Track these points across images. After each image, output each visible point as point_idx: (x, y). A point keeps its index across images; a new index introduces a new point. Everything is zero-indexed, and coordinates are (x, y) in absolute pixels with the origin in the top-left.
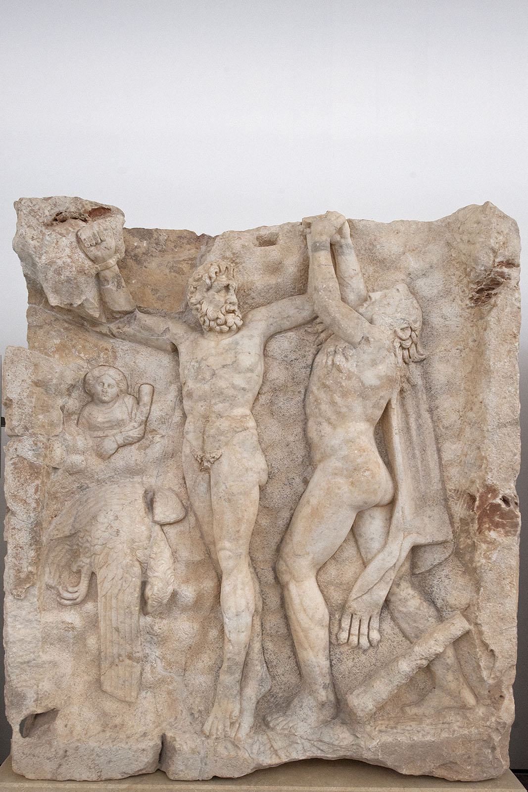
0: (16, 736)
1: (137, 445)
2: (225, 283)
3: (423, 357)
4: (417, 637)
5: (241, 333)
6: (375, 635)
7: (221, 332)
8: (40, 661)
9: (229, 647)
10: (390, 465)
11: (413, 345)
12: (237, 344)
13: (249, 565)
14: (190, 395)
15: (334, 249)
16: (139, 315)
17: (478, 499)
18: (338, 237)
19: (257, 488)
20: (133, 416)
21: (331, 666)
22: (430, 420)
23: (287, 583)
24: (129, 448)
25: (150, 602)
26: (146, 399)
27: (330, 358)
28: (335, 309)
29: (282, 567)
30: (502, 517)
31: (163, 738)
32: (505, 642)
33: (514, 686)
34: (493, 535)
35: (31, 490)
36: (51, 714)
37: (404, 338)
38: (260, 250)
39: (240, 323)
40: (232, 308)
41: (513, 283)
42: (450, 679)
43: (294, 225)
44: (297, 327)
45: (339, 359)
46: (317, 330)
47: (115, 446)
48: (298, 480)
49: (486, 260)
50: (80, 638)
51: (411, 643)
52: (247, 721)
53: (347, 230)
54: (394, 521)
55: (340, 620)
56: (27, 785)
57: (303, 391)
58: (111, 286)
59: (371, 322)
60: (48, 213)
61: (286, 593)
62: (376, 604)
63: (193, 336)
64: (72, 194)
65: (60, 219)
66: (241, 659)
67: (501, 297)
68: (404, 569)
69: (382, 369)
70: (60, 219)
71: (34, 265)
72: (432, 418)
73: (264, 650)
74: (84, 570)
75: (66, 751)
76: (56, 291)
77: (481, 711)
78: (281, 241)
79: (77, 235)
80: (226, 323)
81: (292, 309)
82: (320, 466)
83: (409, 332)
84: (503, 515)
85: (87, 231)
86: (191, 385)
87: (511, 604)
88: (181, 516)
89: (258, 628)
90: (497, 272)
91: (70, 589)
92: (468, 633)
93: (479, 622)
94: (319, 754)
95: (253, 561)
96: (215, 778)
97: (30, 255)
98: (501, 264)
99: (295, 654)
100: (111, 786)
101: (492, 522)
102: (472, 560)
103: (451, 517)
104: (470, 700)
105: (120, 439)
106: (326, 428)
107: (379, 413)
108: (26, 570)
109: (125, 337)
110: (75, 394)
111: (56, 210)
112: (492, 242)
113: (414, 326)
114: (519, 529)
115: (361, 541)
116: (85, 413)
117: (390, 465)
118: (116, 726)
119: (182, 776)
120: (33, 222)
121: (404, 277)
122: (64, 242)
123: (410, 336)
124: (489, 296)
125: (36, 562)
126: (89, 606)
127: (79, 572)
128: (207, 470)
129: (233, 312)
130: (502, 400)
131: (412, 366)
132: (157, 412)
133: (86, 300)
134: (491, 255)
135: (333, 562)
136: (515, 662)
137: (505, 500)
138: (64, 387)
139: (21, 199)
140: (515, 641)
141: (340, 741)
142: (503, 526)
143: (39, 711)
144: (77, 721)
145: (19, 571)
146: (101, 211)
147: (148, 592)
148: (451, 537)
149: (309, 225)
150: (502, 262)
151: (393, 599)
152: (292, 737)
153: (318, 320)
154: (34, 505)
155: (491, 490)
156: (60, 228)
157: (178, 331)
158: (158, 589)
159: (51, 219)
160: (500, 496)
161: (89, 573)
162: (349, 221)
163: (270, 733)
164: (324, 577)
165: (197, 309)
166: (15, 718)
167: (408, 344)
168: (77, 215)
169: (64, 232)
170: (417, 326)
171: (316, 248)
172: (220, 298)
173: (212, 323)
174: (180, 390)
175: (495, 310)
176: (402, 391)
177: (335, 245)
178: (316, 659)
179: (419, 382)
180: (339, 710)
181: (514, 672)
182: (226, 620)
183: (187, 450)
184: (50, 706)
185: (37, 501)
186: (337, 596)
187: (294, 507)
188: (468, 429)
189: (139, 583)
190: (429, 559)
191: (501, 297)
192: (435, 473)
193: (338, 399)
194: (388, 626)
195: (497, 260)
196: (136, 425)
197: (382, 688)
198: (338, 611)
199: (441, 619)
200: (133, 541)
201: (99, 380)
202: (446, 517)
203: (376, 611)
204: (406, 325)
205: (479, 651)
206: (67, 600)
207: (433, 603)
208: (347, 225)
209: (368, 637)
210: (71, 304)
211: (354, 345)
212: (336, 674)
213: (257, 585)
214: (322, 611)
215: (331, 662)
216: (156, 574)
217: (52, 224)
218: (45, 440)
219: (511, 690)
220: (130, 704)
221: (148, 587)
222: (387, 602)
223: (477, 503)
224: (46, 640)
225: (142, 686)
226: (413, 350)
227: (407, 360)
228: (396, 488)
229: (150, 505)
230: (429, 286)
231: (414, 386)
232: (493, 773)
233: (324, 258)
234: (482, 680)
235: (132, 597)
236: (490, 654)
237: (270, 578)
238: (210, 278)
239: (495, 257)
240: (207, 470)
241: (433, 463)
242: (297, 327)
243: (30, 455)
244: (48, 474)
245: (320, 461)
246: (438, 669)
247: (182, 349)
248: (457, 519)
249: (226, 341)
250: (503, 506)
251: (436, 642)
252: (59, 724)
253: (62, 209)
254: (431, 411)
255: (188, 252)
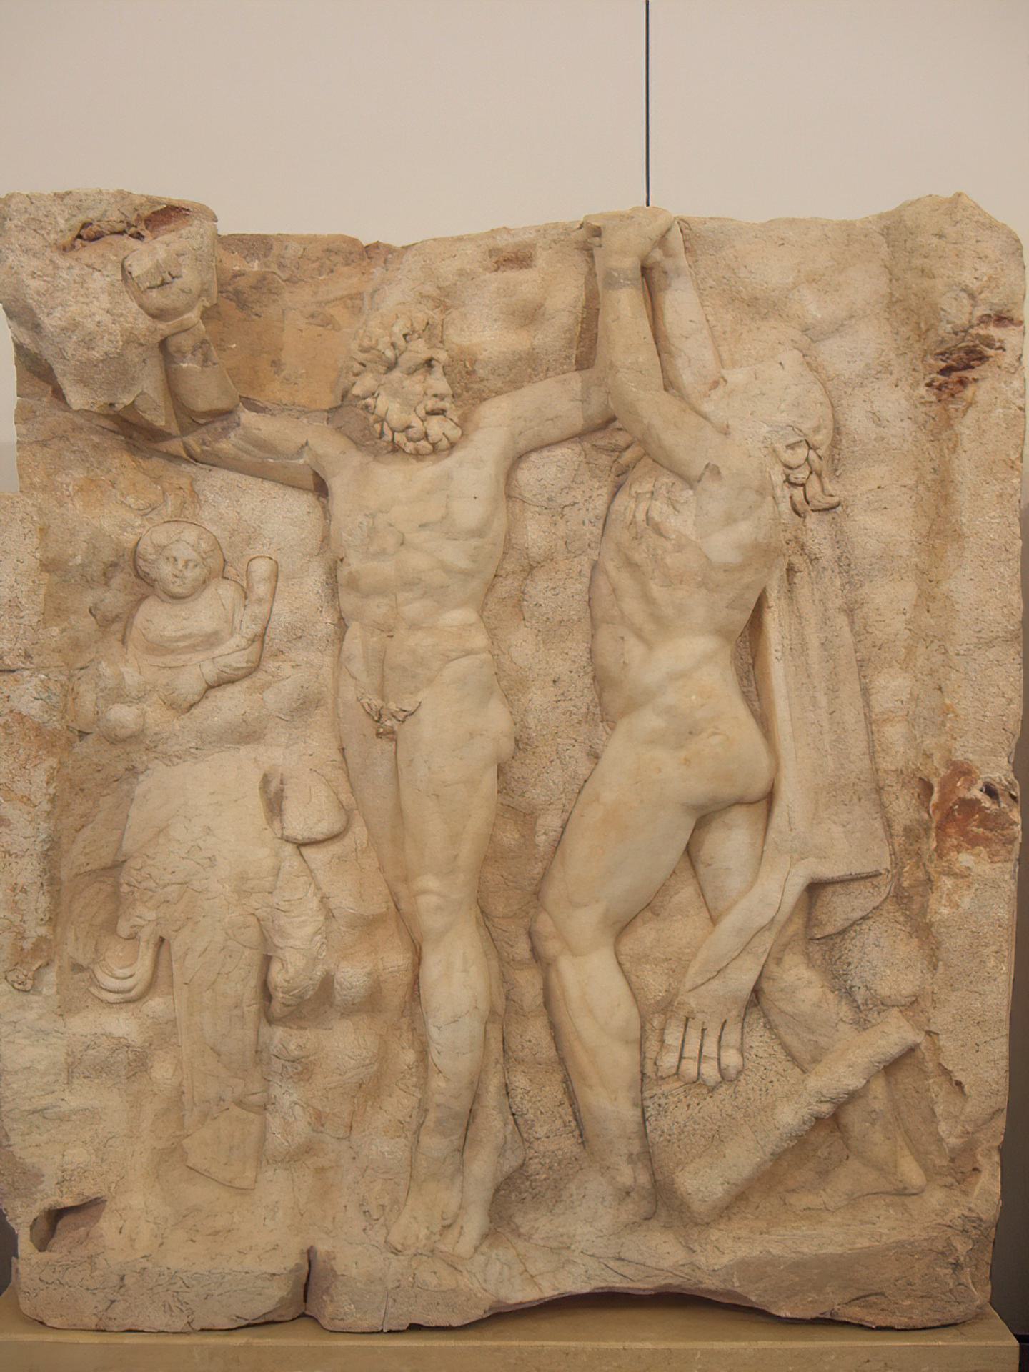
0: (25, 1245)
1: (246, 683)
2: (425, 355)
3: (836, 500)
4: (815, 1061)
5: (458, 455)
6: (732, 1059)
7: (418, 455)
8: (65, 1107)
9: (438, 1083)
10: (764, 721)
11: (814, 477)
12: (449, 477)
13: (478, 922)
14: (353, 584)
15: (650, 279)
16: (247, 417)
17: (936, 789)
18: (657, 255)
19: (493, 772)
20: (237, 624)
21: (644, 1120)
22: (847, 629)
23: (555, 960)
24: (230, 689)
25: (279, 995)
26: (261, 590)
27: (643, 507)
28: (652, 407)
29: (544, 924)
30: (982, 824)
31: (310, 1255)
32: (984, 1066)
33: (1002, 1150)
34: (965, 859)
35: (40, 776)
36: (89, 1208)
37: (794, 463)
38: (495, 281)
39: (455, 433)
40: (441, 405)
41: (1008, 359)
42: (878, 1142)
43: (567, 230)
44: (579, 436)
45: (659, 510)
46: (613, 442)
47: (201, 687)
48: (578, 753)
49: (957, 312)
50: (139, 1064)
51: (804, 1072)
52: (475, 1222)
53: (676, 239)
54: (772, 835)
55: (663, 1030)
56: (51, 1337)
57: (587, 570)
58: (188, 364)
59: (725, 432)
60: (64, 223)
61: (553, 975)
62: (799, 1049)
63: (356, 458)
64: (113, 187)
65: (88, 234)
66: (461, 1105)
67: (984, 385)
68: (791, 930)
69: (745, 530)
70: (88, 234)
71: (36, 327)
72: (852, 623)
73: (507, 1091)
74: (145, 934)
75: (122, 1278)
76: (84, 382)
77: (936, 1198)
78: (541, 259)
79: (123, 266)
80: (426, 436)
81: (560, 399)
82: (623, 726)
83: (802, 452)
84: (988, 821)
85: (145, 257)
86: (355, 563)
87: (996, 994)
88: (337, 828)
89: (495, 1046)
90: (978, 335)
91: (119, 972)
92: (912, 1050)
93: (933, 1028)
94: (618, 1283)
95: (485, 916)
96: (414, 1328)
97: (30, 311)
98: (985, 320)
99: (571, 1097)
100: (212, 1340)
101: (964, 833)
102: (924, 909)
103: (888, 825)
104: (911, 1172)
105: (210, 671)
106: (634, 649)
107: (745, 617)
108: (33, 933)
109: (214, 461)
110: (118, 580)
111: (82, 218)
112: (967, 278)
113: (818, 439)
114: (1017, 846)
115: (702, 869)
116: (139, 619)
117: (764, 721)
118: (217, 1233)
119: (349, 1323)
120: (35, 242)
121: (796, 335)
122: (98, 281)
123: (807, 459)
124: (962, 383)
125: (52, 920)
126: (156, 1004)
127: (133, 937)
128: (391, 735)
129: (442, 412)
130: (981, 592)
131: (812, 520)
132: (283, 614)
133: (142, 393)
134: (965, 301)
135: (648, 914)
136: (1001, 1101)
137: (990, 791)
138: (95, 570)
139: (10, 197)
140: (1004, 1064)
141: (661, 1257)
142: (986, 842)
143: (68, 1202)
144: (136, 1226)
145: (22, 936)
146: (166, 215)
147: (278, 976)
148: (886, 863)
149: (597, 232)
150: (989, 316)
151: (766, 985)
152: (565, 1252)
153: (617, 424)
154: (46, 806)
155: (962, 771)
156: (89, 253)
157: (326, 446)
158: (291, 971)
159: (69, 237)
160: (980, 784)
161: (153, 941)
162: (682, 220)
163: (521, 1245)
164: (628, 946)
165: (367, 407)
166: (23, 1218)
167: (801, 475)
168: (120, 227)
169: (97, 263)
170: (822, 438)
171: (611, 283)
172: (414, 385)
173: (400, 438)
174: (332, 572)
175: (972, 413)
176: (791, 570)
177: (651, 269)
178: (611, 1104)
179: (827, 552)
180: (661, 1201)
181: (1001, 1123)
182: (433, 1031)
183: (349, 693)
184: (87, 1193)
185: (53, 800)
186: (655, 983)
187: (568, 808)
188: (921, 650)
189: (257, 958)
190: (841, 909)
191: (986, 387)
192: (857, 743)
193: (656, 590)
194: (758, 1040)
195: (979, 312)
196: (243, 643)
197: (742, 1158)
198: (655, 1014)
199: (862, 1024)
200: (243, 878)
201: (167, 553)
202: (878, 825)
203: (735, 1013)
204: (798, 438)
205: (937, 1088)
206: (117, 992)
207: (849, 993)
208: (676, 229)
209: (719, 1064)
210: (112, 405)
211: (691, 482)
212: (654, 1137)
213: (494, 963)
214: (622, 1012)
215: (643, 1114)
216: (291, 942)
217: (73, 247)
218: (63, 678)
219: (997, 1158)
220: (243, 1192)
221: (275, 967)
222: (757, 991)
223: (935, 797)
224: (72, 1069)
225: (262, 1157)
226: (814, 488)
227: (799, 507)
228: (776, 768)
229: (274, 804)
230: (841, 356)
231: (814, 559)
232: (957, 1311)
233: (625, 305)
234: (939, 1140)
235: (242, 986)
236: (957, 1089)
237: (521, 949)
238: (393, 345)
239: (974, 306)
240: (391, 735)
241: (851, 716)
242: (579, 436)
243: (33, 709)
244: (70, 743)
245: (623, 714)
246: (855, 1119)
247: (337, 485)
248: (898, 828)
249: (428, 471)
250: (987, 802)
251: (847, 1066)
252: (107, 1225)
253: (92, 215)
254: (850, 611)
255: (347, 281)
